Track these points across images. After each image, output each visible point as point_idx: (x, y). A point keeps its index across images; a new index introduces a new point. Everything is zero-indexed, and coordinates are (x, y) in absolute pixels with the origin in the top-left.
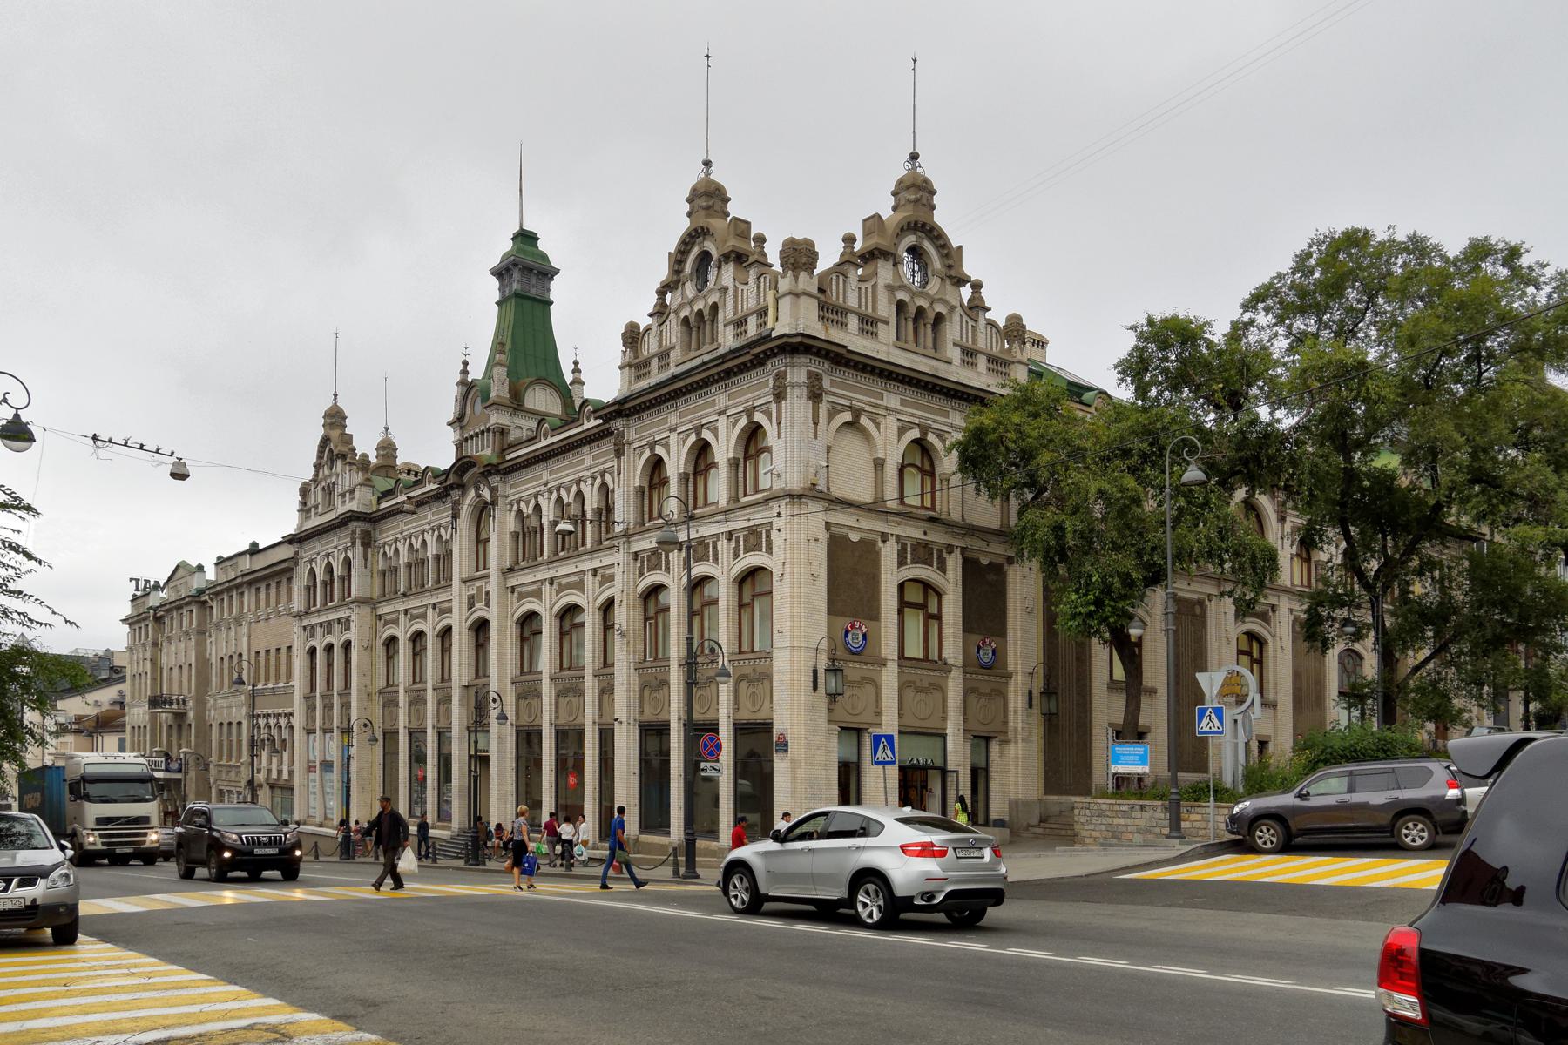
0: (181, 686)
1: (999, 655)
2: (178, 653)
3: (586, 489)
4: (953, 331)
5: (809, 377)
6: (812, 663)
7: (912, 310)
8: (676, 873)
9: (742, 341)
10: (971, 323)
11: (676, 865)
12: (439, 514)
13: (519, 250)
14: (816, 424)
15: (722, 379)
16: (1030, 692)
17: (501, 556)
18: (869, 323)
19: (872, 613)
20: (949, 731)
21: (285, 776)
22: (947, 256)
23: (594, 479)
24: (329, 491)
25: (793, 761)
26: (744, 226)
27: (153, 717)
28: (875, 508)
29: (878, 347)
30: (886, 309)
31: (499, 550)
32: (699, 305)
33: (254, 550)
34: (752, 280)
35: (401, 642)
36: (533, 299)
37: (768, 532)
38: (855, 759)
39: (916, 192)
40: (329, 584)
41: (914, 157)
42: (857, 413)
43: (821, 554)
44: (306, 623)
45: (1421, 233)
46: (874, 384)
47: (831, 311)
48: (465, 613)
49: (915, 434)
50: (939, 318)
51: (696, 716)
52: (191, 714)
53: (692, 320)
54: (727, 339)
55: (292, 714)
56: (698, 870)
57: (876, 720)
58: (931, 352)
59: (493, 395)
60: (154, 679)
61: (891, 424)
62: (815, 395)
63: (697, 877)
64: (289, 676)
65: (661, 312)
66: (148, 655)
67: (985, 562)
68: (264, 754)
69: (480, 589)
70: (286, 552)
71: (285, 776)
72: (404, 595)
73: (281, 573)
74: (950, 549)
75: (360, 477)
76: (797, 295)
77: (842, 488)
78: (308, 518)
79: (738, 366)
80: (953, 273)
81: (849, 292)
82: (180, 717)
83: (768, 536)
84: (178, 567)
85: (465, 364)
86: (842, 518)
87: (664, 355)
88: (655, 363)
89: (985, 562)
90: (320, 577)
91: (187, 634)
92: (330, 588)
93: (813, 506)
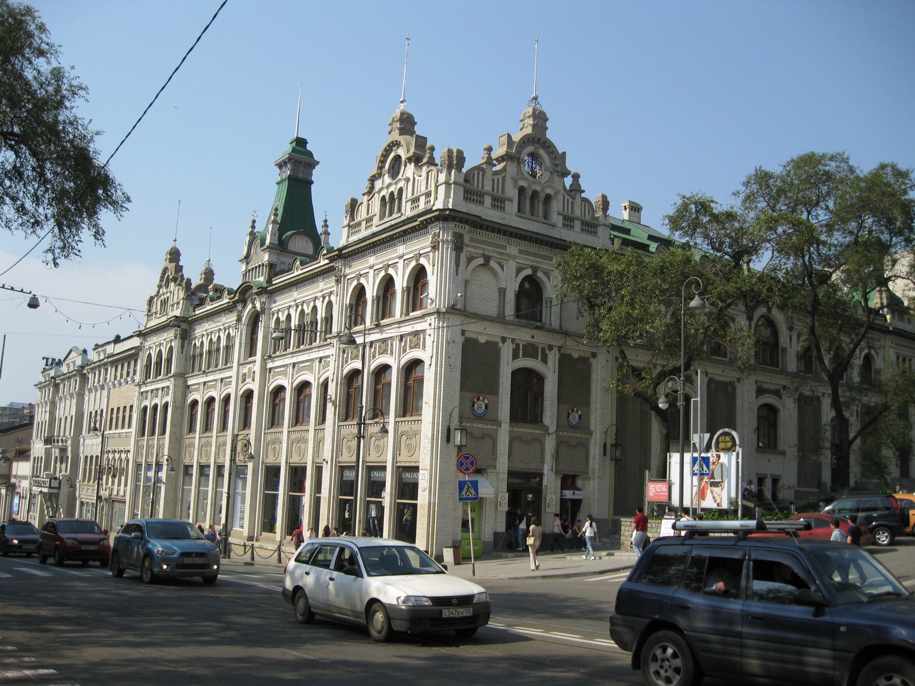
1: (584, 420)
4: (556, 206)
6: (446, 424)
7: (529, 193)
9: (416, 212)
10: (570, 200)
12: (232, 318)
13: (294, 149)
15: (402, 236)
16: (605, 445)
19: (492, 389)
20: (545, 472)
21: (122, 493)
23: (324, 297)
24: (164, 303)
27: (48, 453)
30: (511, 192)
32: (392, 188)
33: (118, 340)
34: (424, 174)
37: (424, 336)
40: (159, 363)
41: (535, 98)
42: (487, 259)
44: (143, 389)
45: (369, 177)
46: (500, 240)
49: (528, 272)
50: (548, 198)
52: (69, 449)
53: (387, 198)
54: (408, 211)
55: (129, 451)
58: (543, 220)
61: (511, 266)
65: (371, 191)
70: (136, 342)
71: (122, 493)
72: (204, 372)
73: (132, 356)
74: (551, 347)
77: (475, 306)
79: (411, 228)
80: (559, 169)
82: (63, 450)
83: (424, 339)
84: (71, 351)
85: (254, 222)
87: (369, 220)
88: (364, 223)
90: (154, 360)
91: (71, 396)
92: (156, 367)
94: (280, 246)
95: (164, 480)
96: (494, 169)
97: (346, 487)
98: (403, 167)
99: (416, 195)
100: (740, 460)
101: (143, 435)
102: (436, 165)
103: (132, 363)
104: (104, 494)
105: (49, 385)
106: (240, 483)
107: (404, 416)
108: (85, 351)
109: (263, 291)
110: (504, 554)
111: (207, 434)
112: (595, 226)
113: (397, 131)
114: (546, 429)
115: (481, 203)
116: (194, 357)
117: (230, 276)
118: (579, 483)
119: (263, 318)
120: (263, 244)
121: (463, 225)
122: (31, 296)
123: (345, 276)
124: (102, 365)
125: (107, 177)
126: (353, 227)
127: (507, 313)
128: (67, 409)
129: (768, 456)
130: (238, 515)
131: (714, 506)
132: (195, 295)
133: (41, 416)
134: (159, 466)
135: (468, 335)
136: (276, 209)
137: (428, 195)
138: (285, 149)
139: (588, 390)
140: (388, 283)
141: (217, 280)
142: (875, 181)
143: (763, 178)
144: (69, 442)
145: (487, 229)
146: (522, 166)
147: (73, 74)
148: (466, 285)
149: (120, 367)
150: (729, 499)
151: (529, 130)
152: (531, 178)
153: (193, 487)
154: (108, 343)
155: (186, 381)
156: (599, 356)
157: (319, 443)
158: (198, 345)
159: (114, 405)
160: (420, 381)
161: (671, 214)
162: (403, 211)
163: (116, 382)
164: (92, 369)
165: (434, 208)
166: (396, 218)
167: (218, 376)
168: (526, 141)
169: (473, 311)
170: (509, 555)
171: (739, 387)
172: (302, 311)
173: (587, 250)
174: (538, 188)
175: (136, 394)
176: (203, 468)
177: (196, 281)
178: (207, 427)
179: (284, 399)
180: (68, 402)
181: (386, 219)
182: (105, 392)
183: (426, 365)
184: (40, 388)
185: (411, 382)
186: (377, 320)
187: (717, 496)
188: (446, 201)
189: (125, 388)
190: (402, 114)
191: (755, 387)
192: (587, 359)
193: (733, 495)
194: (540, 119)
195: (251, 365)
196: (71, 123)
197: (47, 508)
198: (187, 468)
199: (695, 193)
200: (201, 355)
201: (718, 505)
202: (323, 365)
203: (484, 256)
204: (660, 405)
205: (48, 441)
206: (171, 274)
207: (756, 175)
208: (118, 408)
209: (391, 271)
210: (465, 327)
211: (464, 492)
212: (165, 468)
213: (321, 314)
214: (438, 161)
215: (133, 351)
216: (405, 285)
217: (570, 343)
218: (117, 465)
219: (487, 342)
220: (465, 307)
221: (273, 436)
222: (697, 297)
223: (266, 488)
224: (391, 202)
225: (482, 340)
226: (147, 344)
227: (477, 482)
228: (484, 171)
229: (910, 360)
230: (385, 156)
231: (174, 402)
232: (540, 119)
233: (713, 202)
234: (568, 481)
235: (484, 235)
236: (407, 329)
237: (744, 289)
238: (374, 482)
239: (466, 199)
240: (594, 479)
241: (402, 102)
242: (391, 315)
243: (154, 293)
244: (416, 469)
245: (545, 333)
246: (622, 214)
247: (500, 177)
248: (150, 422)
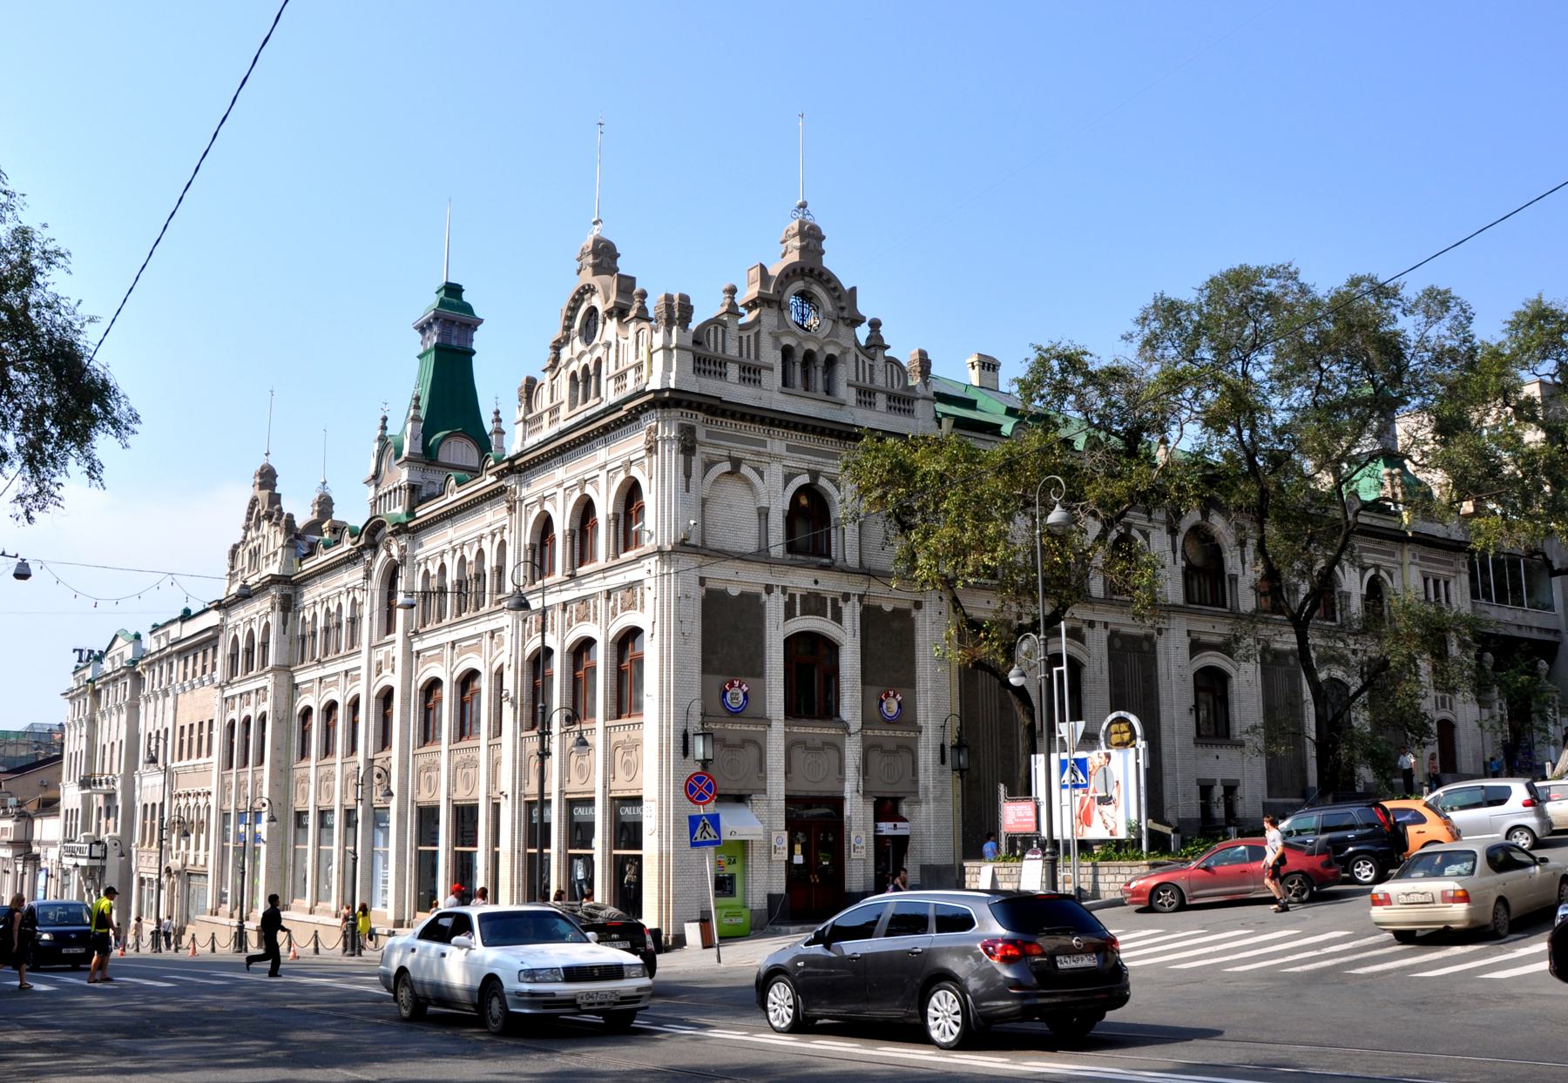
4: (844, 373)
6: (682, 728)
7: (799, 356)
10: (868, 362)
12: (353, 576)
13: (442, 303)
16: (943, 747)
18: (751, 373)
19: (755, 668)
20: (847, 795)
21: (201, 861)
23: (494, 535)
24: (254, 554)
27: (87, 801)
29: (766, 394)
30: (771, 356)
32: (586, 360)
33: (187, 616)
40: (249, 651)
41: (803, 206)
42: (736, 463)
44: (229, 692)
46: (755, 431)
49: (804, 479)
50: (831, 361)
53: (579, 375)
54: (610, 394)
58: (823, 395)
61: (775, 472)
67: (888, 608)
68: (174, 837)
70: (213, 618)
71: (201, 861)
73: (208, 641)
74: (846, 597)
80: (845, 314)
81: (728, 343)
82: (110, 797)
85: (385, 419)
89: (888, 608)
90: (242, 645)
91: (119, 708)
94: (427, 456)
95: (264, 836)
96: (741, 321)
97: (536, 833)
98: (600, 326)
99: (621, 368)
100: (1141, 761)
101: (231, 766)
102: (650, 320)
103: (210, 651)
104: (175, 864)
105: (84, 693)
106: (380, 836)
107: (619, 717)
108: (138, 637)
109: (401, 529)
110: (784, 928)
111: (328, 760)
112: (910, 401)
113: (590, 270)
114: (845, 727)
115: (723, 375)
116: (303, 638)
117: (353, 511)
118: (904, 809)
119: (403, 572)
120: (398, 455)
121: (695, 412)
122: (18, 560)
123: (521, 501)
124: (164, 658)
125: (105, 383)
126: (529, 422)
127: (772, 542)
128: (113, 730)
129: (1216, 751)
130: (380, 886)
131: (1106, 835)
132: (300, 540)
133: (74, 744)
134: (257, 816)
135: (710, 585)
136: (417, 399)
137: (639, 367)
138: (427, 302)
139: (911, 662)
140: (586, 509)
141: (337, 516)
142: (1342, 306)
143: (1169, 311)
144: (118, 784)
145: (733, 416)
146: (786, 313)
147: (47, 233)
148: (703, 505)
149: (191, 659)
150: (1129, 822)
151: (794, 257)
152: (801, 332)
153: (310, 847)
154: (172, 622)
156: (927, 606)
157: (494, 765)
158: (309, 618)
159: (184, 720)
160: (639, 662)
161: (1021, 376)
162: (603, 394)
163: (186, 684)
164: (150, 664)
165: (648, 389)
166: (593, 406)
167: (341, 667)
168: (790, 274)
169: (717, 546)
170: (792, 929)
171: (1161, 643)
172: (463, 559)
173: (890, 441)
174: (814, 347)
175: (218, 701)
176: (323, 814)
177: (303, 515)
178: (328, 750)
179: (440, 700)
180: (114, 719)
181: (579, 408)
182: (170, 701)
183: (646, 635)
184: (71, 699)
185: (626, 663)
186: (573, 568)
187: (1109, 821)
188: (665, 377)
189: (199, 692)
190: (596, 242)
191: (1187, 641)
192: (908, 612)
193: (1134, 817)
194: (811, 238)
195: (389, 648)
196: (49, 307)
197: (89, 890)
198: (300, 816)
199: (1056, 341)
200: (314, 634)
201: (1111, 833)
202: (493, 645)
203: (730, 458)
204: (1012, 681)
205: (86, 783)
206: (263, 507)
207: (1155, 306)
208: (192, 726)
209: (589, 490)
210: (706, 572)
211: (698, 834)
212: (265, 817)
213: (490, 562)
214: (651, 314)
215: (210, 633)
216: (610, 511)
217: (876, 588)
218: (184, 814)
219: (742, 594)
220: (703, 541)
221: (427, 759)
222: (1058, 507)
223: (420, 842)
224: (585, 381)
225: (734, 591)
226: (230, 621)
227: (717, 816)
228: (724, 325)
229: (1446, 583)
230: (573, 309)
231: (276, 711)
232: (811, 238)
233: (1085, 353)
234: (886, 808)
235: (729, 427)
237: (1141, 488)
238: (578, 824)
239: (697, 370)
240: (927, 803)
241: (595, 223)
242: (593, 559)
243: (238, 540)
244: (637, 801)
245: (836, 575)
246: (968, 376)
247: (752, 333)
248: (240, 743)
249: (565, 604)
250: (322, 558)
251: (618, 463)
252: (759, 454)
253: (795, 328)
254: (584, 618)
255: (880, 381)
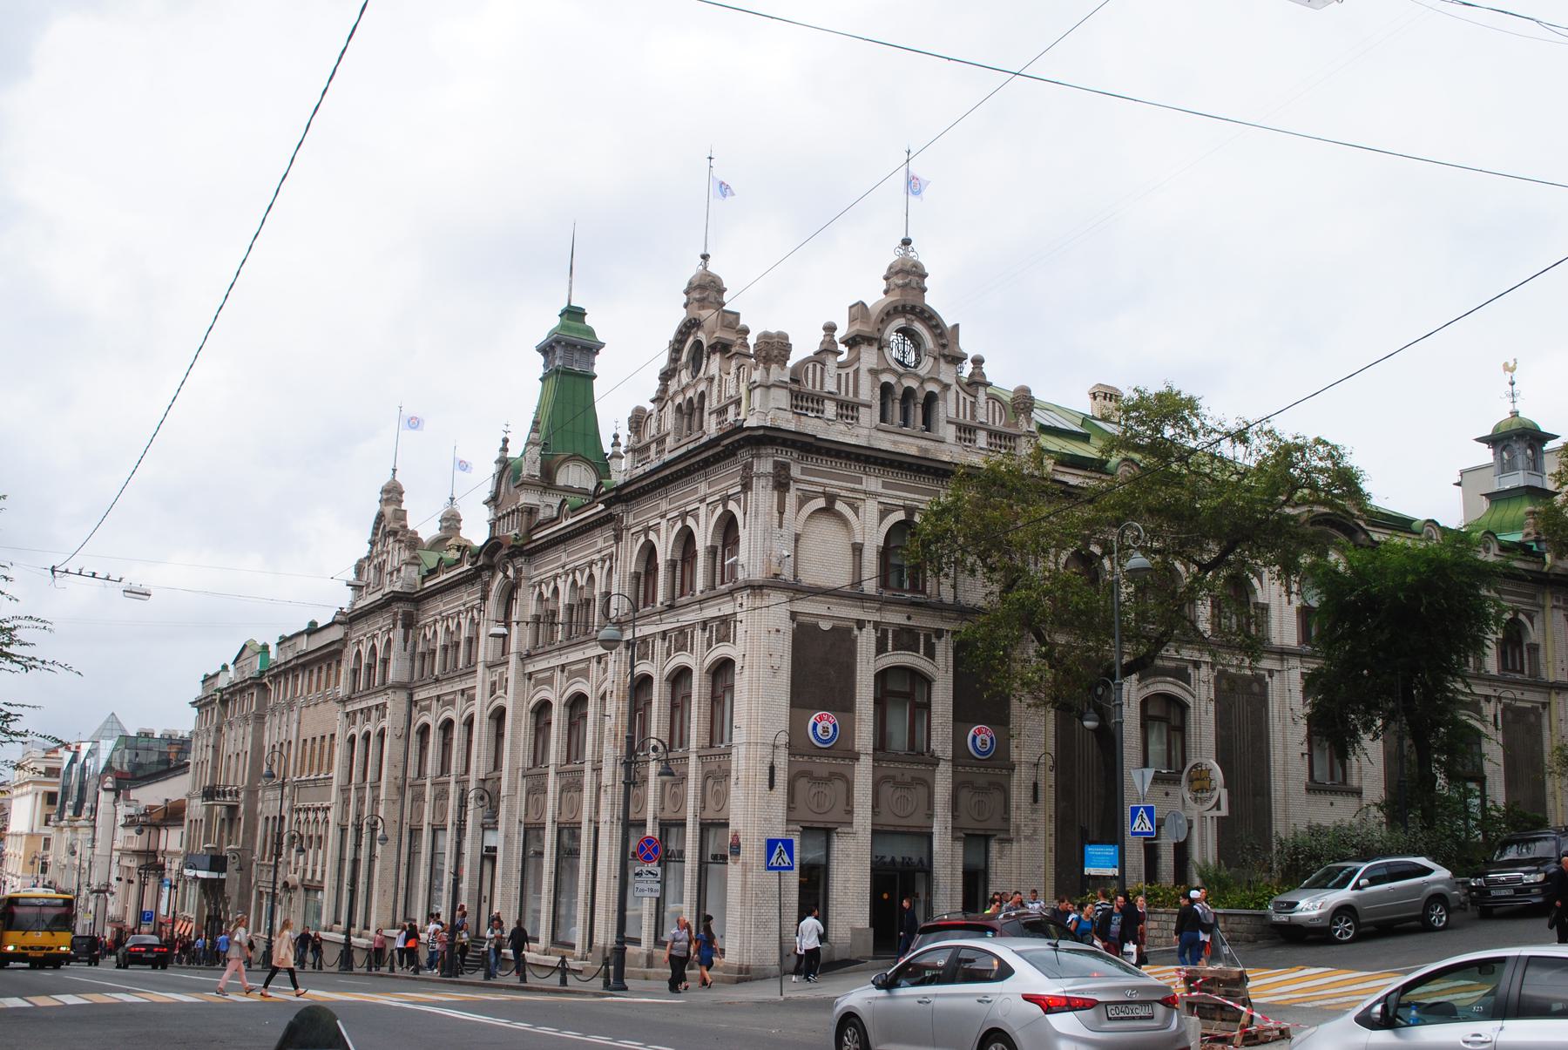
0: (237, 776)
2: (238, 739)
3: (596, 570)
4: (947, 408)
5: (775, 468)
6: (769, 759)
8: (607, 984)
10: (969, 399)
11: (607, 975)
12: (469, 596)
13: (562, 326)
14: (781, 513)
17: (520, 641)
18: (849, 409)
19: (843, 703)
20: (936, 829)
22: (941, 335)
23: (604, 561)
24: (380, 568)
25: (744, 864)
26: (731, 317)
27: (210, 809)
28: (854, 595)
30: (867, 391)
31: (519, 638)
32: (690, 393)
33: (313, 630)
34: (733, 371)
35: (591, 701)
36: (576, 374)
38: (823, 861)
39: (907, 277)
41: (906, 242)
42: (831, 499)
43: (784, 646)
44: (349, 709)
46: (854, 470)
47: (803, 399)
48: (487, 700)
49: (900, 516)
50: (931, 399)
51: (632, 817)
54: (712, 427)
56: (627, 982)
57: (847, 818)
59: (525, 472)
60: (214, 768)
61: (871, 508)
62: (781, 483)
63: (626, 989)
64: (330, 767)
66: (211, 741)
69: (501, 674)
70: (336, 633)
71: (318, 877)
73: (330, 656)
74: (939, 633)
75: (406, 555)
76: (768, 387)
77: (812, 575)
78: (360, 597)
80: (946, 352)
81: (827, 379)
82: (232, 810)
84: (245, 646)
85: (506, 441)
86: (807, 607)
88: (653, 446)
90: (365, 660)
91: (246, 719)
93: (776, 597)
127: (865, 575)
135: (800, 618)
137: (738, 403)
148: (797, 541)
152: (900, 369)
155: (411, 695)
159: (307, 733)
168: (890, 313)
174: (914, 384)
175: (339, 716)
182: (295, 716)
184: (199, 708)
220: (795, 576)
225: (825, 626)
235: (825, 465)
236: (711, 612)
238: (1112, 842)
240: (1019, 841)
243: (364, 554)
249: (664, 633)
250: (443, 577)
251: (717, 497)
252: (853, 490)
253: (894, 365)
254: (681, 647)
255: (982, 416)
